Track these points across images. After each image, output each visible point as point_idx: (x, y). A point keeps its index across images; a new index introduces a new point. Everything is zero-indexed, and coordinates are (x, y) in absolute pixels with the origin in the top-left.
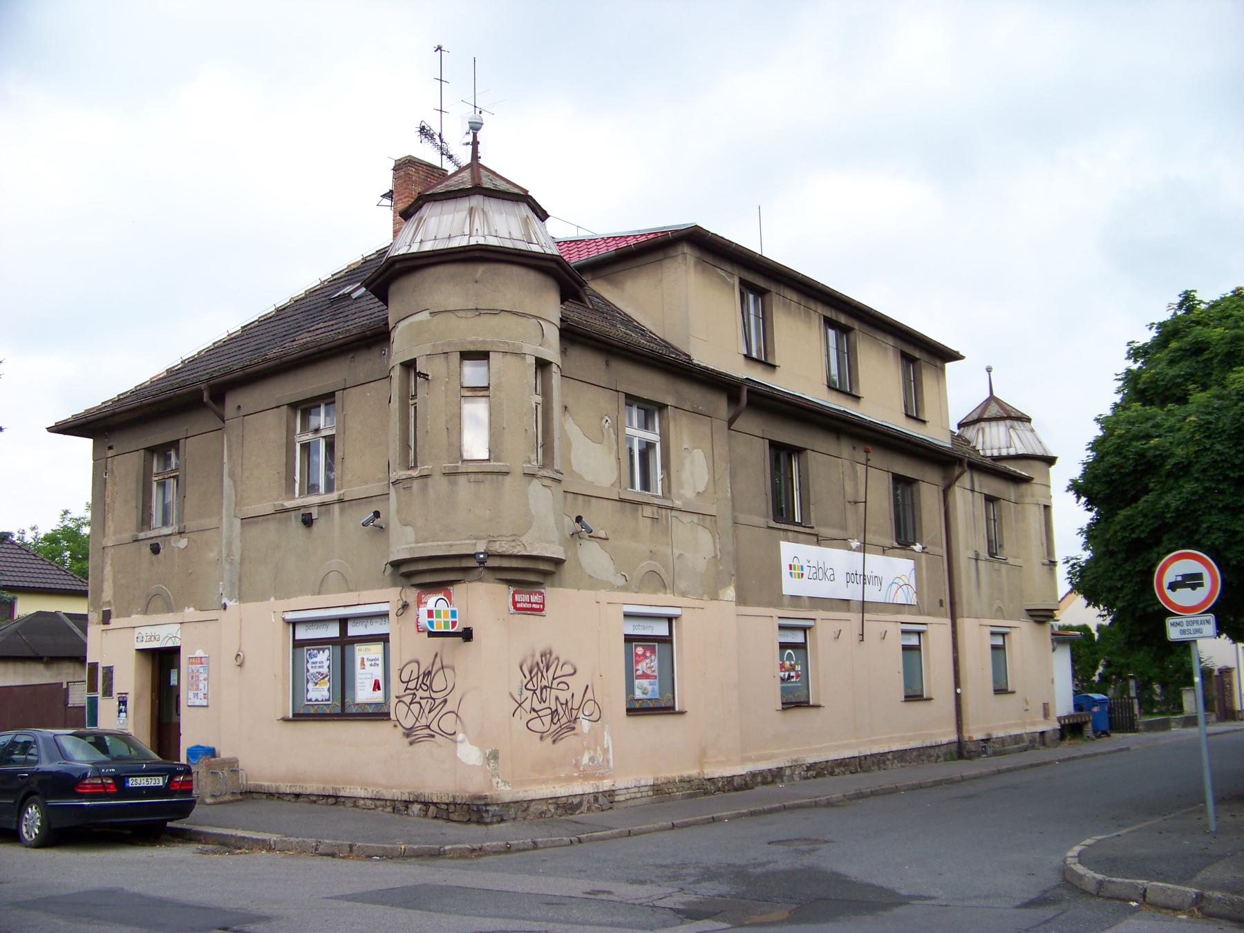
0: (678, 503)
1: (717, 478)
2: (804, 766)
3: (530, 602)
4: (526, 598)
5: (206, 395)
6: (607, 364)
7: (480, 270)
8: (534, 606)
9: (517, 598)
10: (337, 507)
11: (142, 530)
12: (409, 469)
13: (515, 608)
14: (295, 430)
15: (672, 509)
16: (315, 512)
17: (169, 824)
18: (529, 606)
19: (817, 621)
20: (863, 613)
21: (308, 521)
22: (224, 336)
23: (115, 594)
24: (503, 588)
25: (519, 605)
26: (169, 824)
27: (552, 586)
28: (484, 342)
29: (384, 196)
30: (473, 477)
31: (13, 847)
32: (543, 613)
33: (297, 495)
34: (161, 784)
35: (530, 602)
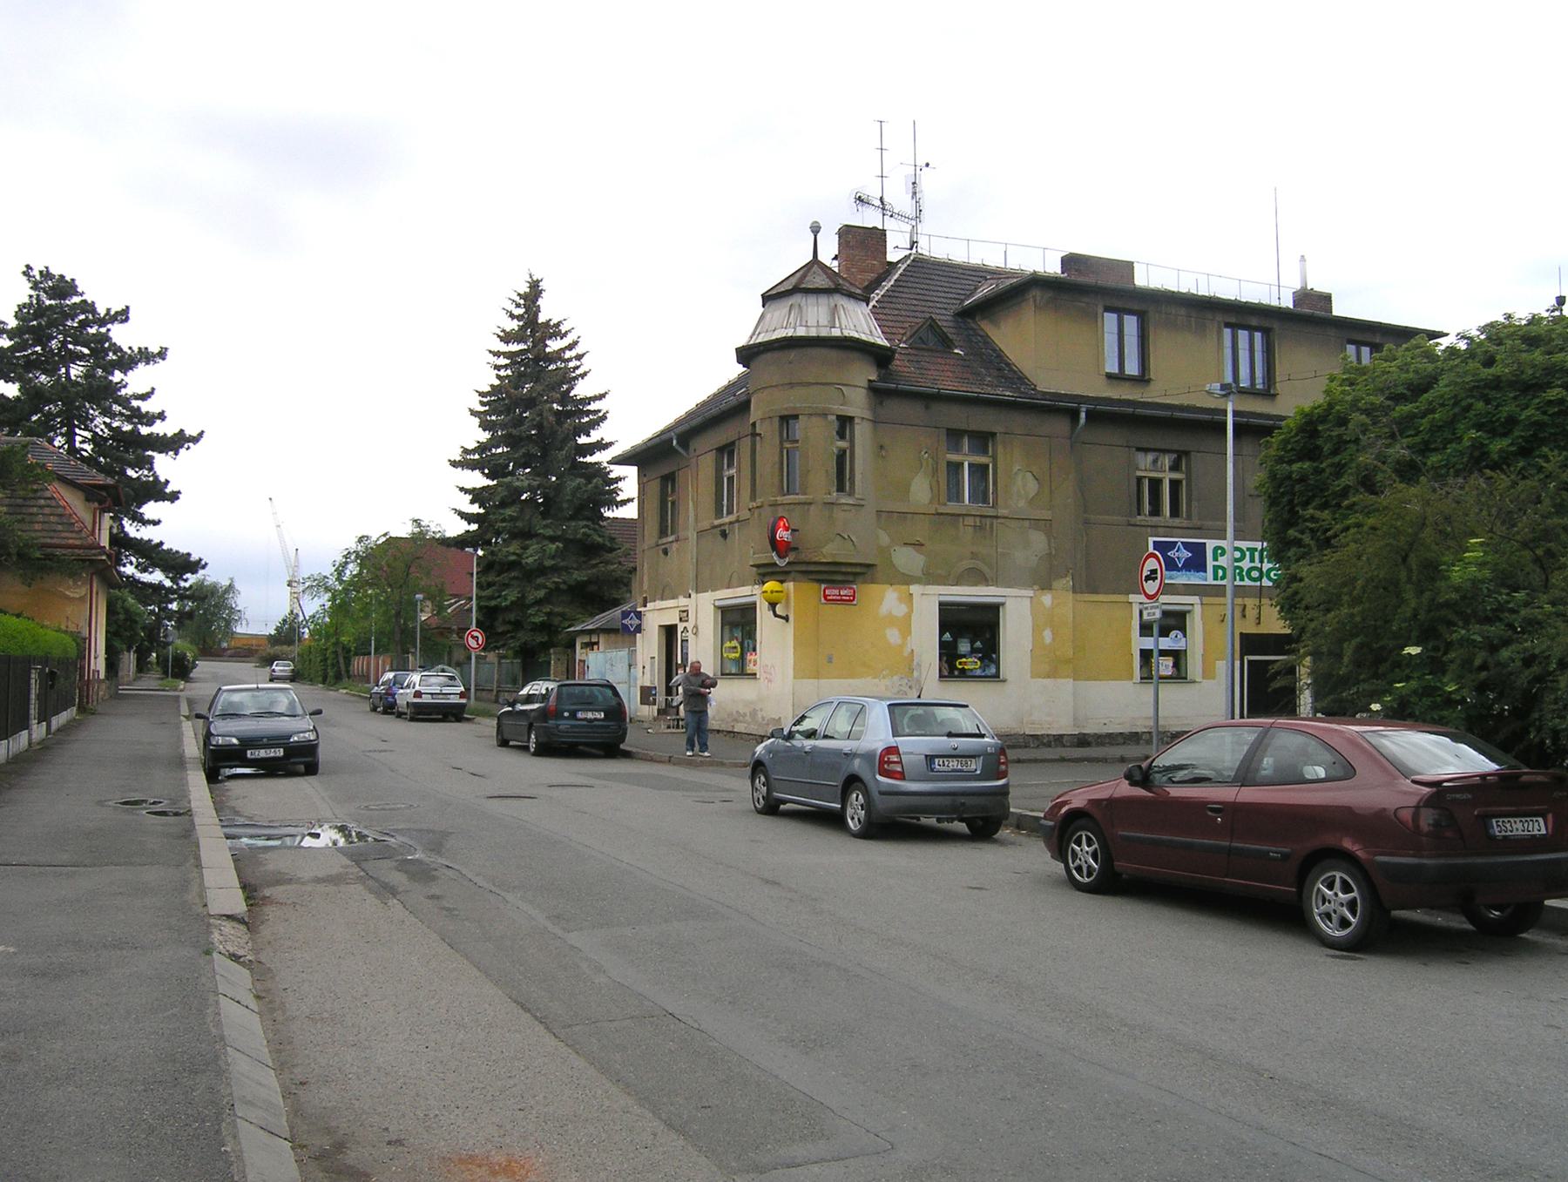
0: (1002, 512)
1: (1053, 488)
2: (1169, 734)
3: (840, 595)
4: (837, 592)
5: (675, 442)
6: (927, 408)
7: (793, 354)
8: (844, 598)
9: (827, 592)
10: (736, 525)
11: (660, 538)
12: (784, 495)
13: (826, 599)
14: (723, 467)
15: (997, 517)
16: (726, 528)
17: (1547, 902)
18: (839, 598)
19: (1195, 606)
20: (1260, 598)
21: (724, 535)
22: (725, 383)
23: (649, 587)
24: (816, 585)
25: (829, 598)
26: (1547, 902)
27: (865, 582)
28: (795, 408)
29: (833, 259)
30: (787, 507)
31: (936, 847)
32: (855, 602)
33: (725, 515)
34: (1543, 831)
35: (840, 595)
